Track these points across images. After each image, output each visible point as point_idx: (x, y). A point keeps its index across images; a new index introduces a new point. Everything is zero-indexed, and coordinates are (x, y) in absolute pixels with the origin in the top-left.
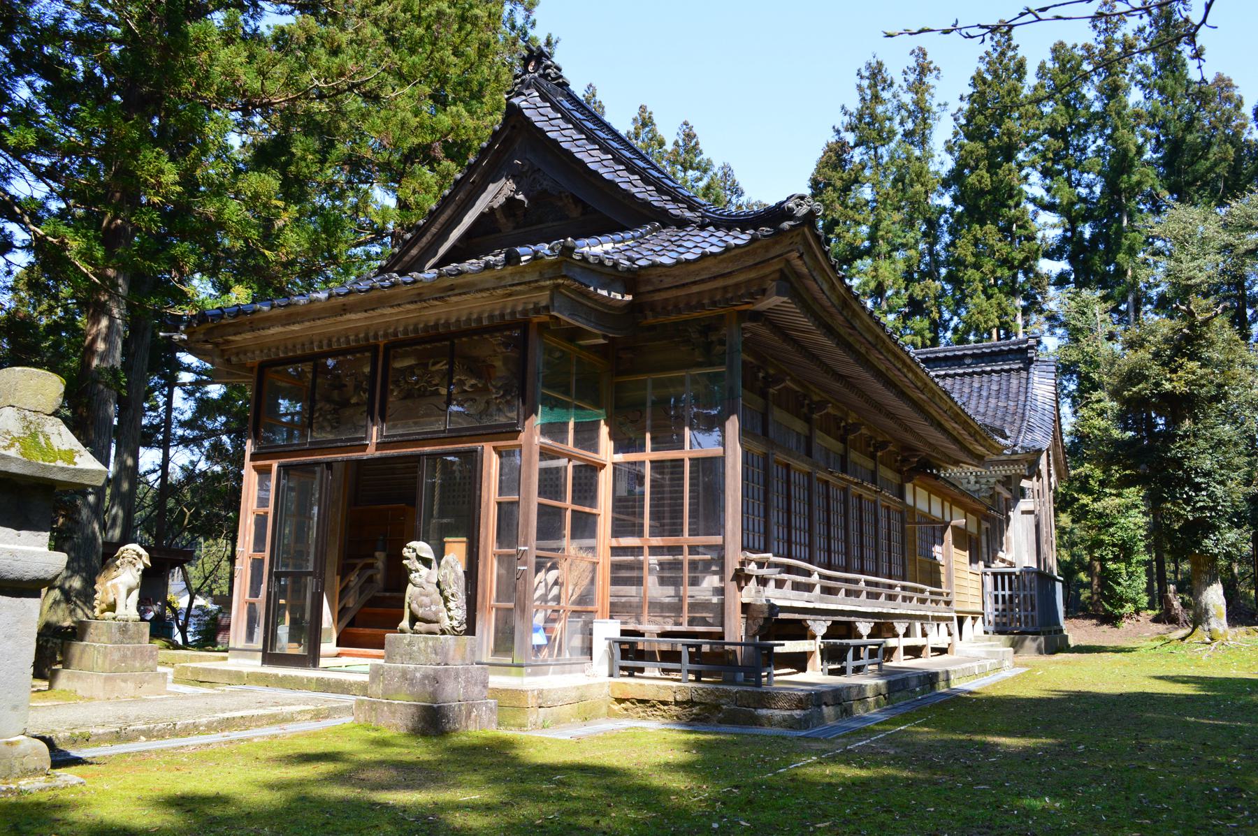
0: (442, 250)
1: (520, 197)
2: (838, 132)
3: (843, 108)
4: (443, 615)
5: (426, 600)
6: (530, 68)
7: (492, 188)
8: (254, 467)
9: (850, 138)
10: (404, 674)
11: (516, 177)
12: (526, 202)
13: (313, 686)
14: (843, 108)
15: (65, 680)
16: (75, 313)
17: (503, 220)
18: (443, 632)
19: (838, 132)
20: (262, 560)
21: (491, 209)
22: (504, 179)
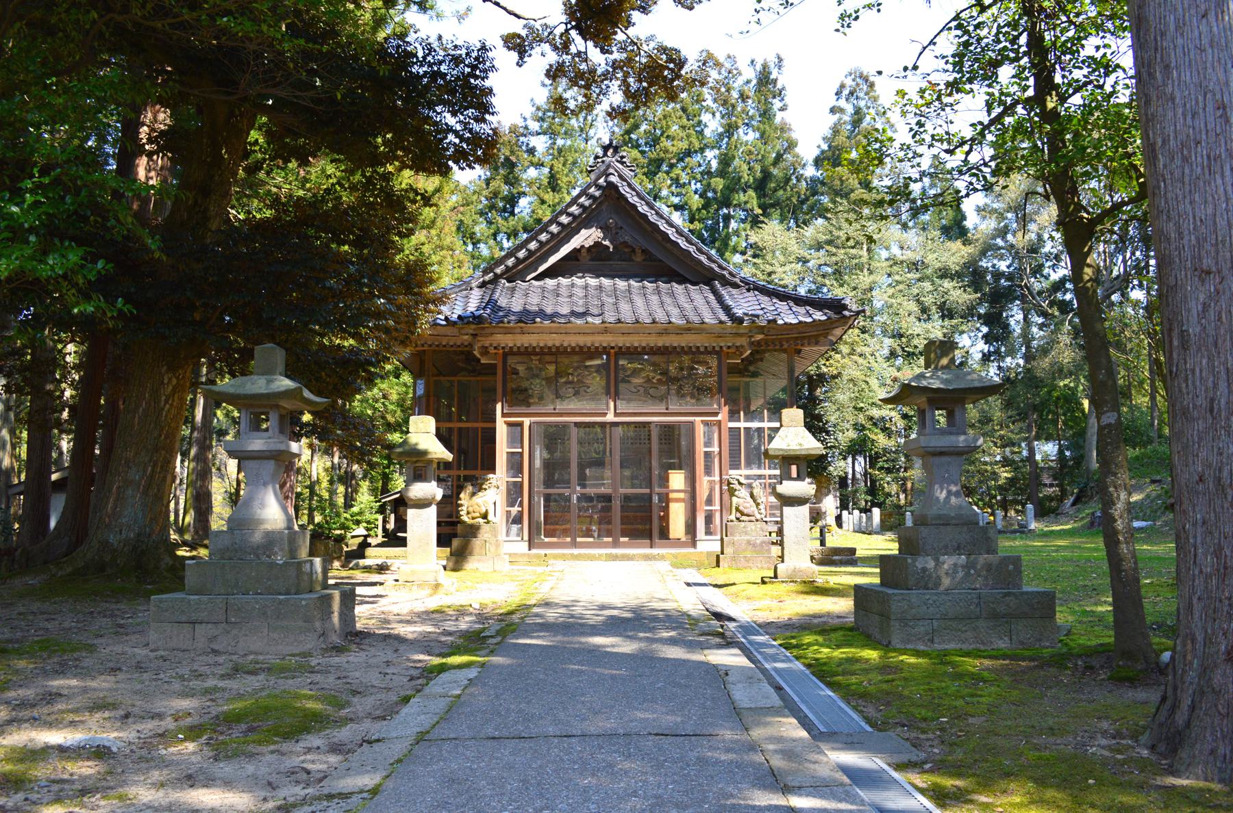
0: (542, 269)
1: (607, 243)
2: (525, 119)
3: (532, 100)
4: (756, 512)
5: (748, 505)
6: (609, 154)
7: (584, 233)
8: (505, 422)
9: (534, 126)
10: (749, 542)
11: (605, 229)
12: (611, 247)
13: (604, 558)
14: (532, 100)
15: (472, 564)
16: (409, 308)
17: (585, 254)
18: (757, 520)
19: (525, 119)
20: (522, 483)
21: (583, 247)
22: (594, 229)
